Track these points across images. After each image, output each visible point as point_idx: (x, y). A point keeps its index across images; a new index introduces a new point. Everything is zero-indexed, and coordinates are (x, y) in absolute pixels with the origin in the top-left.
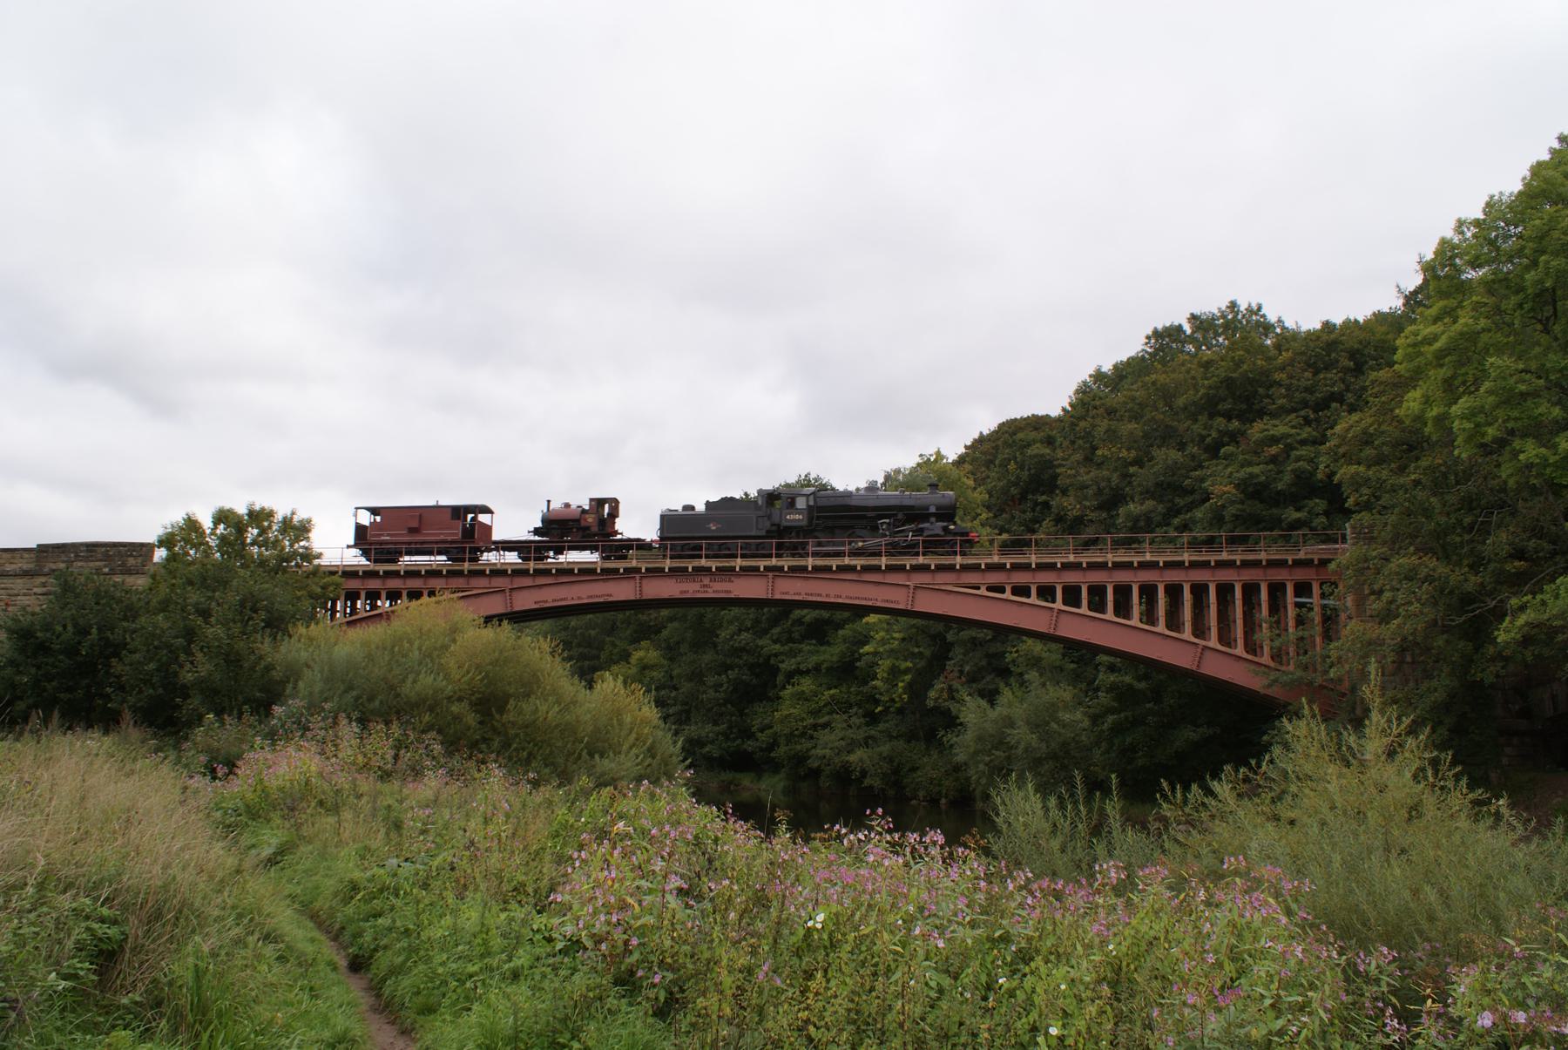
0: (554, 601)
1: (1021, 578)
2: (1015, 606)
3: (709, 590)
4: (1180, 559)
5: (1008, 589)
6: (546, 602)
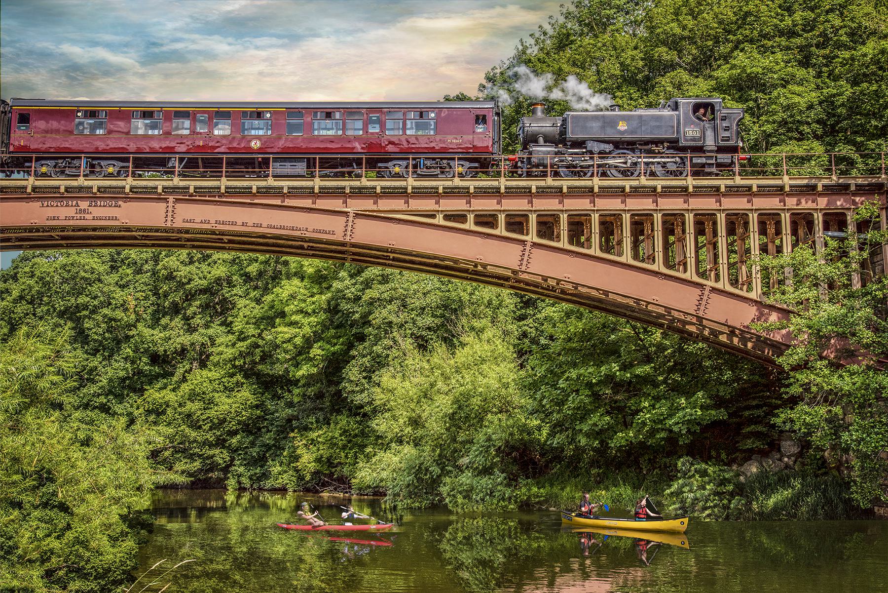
0: (270, 227)
1: (488, 205)
2: (478, 240)
3: (87, 216)
4: (778, 182)
5: (471, 217)
6: (234, 224)
